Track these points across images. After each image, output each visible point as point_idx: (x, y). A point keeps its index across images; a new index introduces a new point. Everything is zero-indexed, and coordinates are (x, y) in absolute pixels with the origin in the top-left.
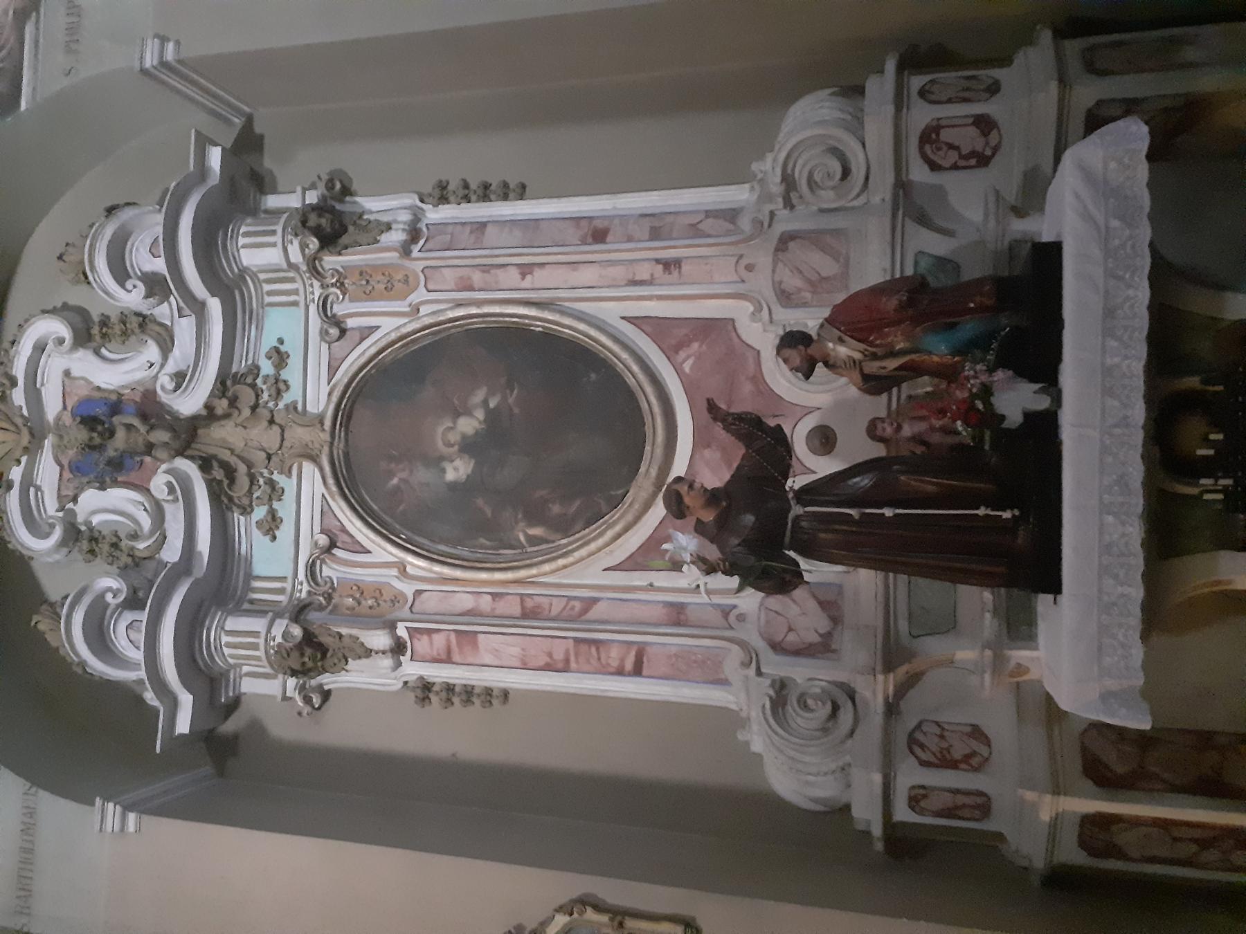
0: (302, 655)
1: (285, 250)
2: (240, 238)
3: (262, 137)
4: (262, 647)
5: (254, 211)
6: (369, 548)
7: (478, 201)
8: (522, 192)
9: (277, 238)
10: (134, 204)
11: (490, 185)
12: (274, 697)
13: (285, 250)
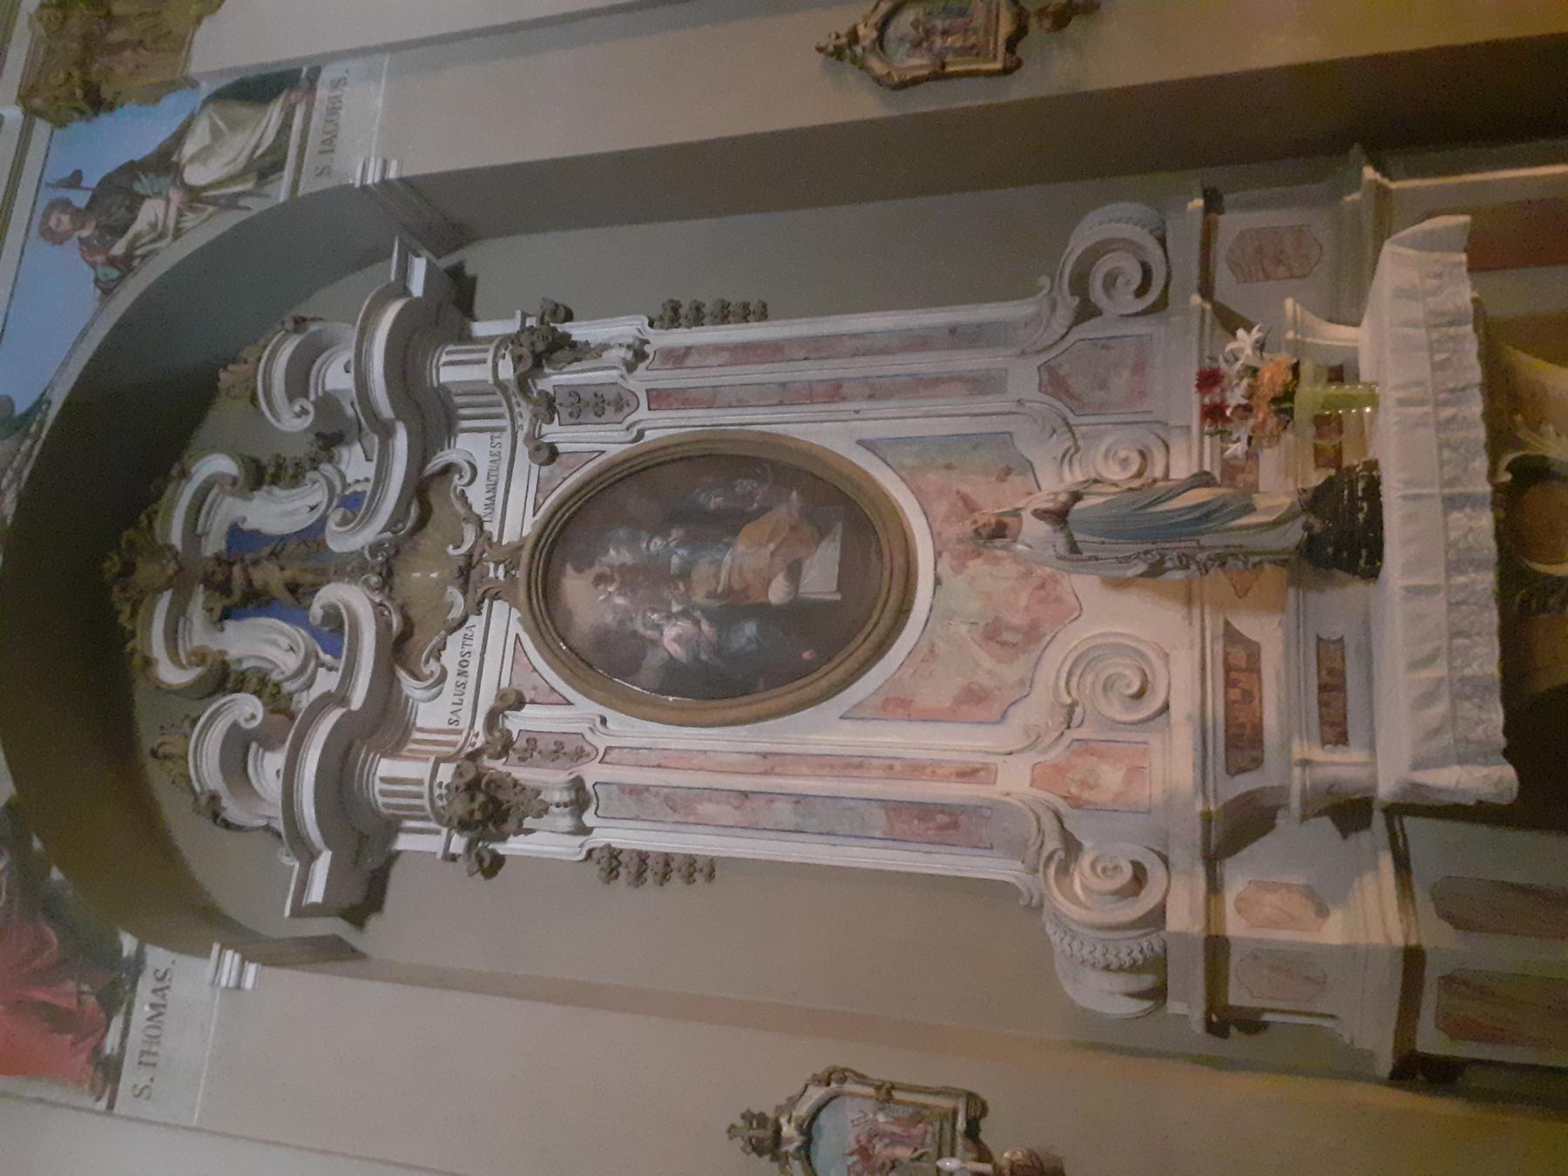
0: (472, 799)
1: (495, 366)
2: (444, 354)
3: (474, 280)
4: (426, 795)
5: (465, 337)
6: (571, 699)
7: (713, 324)
8: (763, 315)
9: (490, 356)
10: (321, 319)
11: (729, 304)
13: (495, 366)
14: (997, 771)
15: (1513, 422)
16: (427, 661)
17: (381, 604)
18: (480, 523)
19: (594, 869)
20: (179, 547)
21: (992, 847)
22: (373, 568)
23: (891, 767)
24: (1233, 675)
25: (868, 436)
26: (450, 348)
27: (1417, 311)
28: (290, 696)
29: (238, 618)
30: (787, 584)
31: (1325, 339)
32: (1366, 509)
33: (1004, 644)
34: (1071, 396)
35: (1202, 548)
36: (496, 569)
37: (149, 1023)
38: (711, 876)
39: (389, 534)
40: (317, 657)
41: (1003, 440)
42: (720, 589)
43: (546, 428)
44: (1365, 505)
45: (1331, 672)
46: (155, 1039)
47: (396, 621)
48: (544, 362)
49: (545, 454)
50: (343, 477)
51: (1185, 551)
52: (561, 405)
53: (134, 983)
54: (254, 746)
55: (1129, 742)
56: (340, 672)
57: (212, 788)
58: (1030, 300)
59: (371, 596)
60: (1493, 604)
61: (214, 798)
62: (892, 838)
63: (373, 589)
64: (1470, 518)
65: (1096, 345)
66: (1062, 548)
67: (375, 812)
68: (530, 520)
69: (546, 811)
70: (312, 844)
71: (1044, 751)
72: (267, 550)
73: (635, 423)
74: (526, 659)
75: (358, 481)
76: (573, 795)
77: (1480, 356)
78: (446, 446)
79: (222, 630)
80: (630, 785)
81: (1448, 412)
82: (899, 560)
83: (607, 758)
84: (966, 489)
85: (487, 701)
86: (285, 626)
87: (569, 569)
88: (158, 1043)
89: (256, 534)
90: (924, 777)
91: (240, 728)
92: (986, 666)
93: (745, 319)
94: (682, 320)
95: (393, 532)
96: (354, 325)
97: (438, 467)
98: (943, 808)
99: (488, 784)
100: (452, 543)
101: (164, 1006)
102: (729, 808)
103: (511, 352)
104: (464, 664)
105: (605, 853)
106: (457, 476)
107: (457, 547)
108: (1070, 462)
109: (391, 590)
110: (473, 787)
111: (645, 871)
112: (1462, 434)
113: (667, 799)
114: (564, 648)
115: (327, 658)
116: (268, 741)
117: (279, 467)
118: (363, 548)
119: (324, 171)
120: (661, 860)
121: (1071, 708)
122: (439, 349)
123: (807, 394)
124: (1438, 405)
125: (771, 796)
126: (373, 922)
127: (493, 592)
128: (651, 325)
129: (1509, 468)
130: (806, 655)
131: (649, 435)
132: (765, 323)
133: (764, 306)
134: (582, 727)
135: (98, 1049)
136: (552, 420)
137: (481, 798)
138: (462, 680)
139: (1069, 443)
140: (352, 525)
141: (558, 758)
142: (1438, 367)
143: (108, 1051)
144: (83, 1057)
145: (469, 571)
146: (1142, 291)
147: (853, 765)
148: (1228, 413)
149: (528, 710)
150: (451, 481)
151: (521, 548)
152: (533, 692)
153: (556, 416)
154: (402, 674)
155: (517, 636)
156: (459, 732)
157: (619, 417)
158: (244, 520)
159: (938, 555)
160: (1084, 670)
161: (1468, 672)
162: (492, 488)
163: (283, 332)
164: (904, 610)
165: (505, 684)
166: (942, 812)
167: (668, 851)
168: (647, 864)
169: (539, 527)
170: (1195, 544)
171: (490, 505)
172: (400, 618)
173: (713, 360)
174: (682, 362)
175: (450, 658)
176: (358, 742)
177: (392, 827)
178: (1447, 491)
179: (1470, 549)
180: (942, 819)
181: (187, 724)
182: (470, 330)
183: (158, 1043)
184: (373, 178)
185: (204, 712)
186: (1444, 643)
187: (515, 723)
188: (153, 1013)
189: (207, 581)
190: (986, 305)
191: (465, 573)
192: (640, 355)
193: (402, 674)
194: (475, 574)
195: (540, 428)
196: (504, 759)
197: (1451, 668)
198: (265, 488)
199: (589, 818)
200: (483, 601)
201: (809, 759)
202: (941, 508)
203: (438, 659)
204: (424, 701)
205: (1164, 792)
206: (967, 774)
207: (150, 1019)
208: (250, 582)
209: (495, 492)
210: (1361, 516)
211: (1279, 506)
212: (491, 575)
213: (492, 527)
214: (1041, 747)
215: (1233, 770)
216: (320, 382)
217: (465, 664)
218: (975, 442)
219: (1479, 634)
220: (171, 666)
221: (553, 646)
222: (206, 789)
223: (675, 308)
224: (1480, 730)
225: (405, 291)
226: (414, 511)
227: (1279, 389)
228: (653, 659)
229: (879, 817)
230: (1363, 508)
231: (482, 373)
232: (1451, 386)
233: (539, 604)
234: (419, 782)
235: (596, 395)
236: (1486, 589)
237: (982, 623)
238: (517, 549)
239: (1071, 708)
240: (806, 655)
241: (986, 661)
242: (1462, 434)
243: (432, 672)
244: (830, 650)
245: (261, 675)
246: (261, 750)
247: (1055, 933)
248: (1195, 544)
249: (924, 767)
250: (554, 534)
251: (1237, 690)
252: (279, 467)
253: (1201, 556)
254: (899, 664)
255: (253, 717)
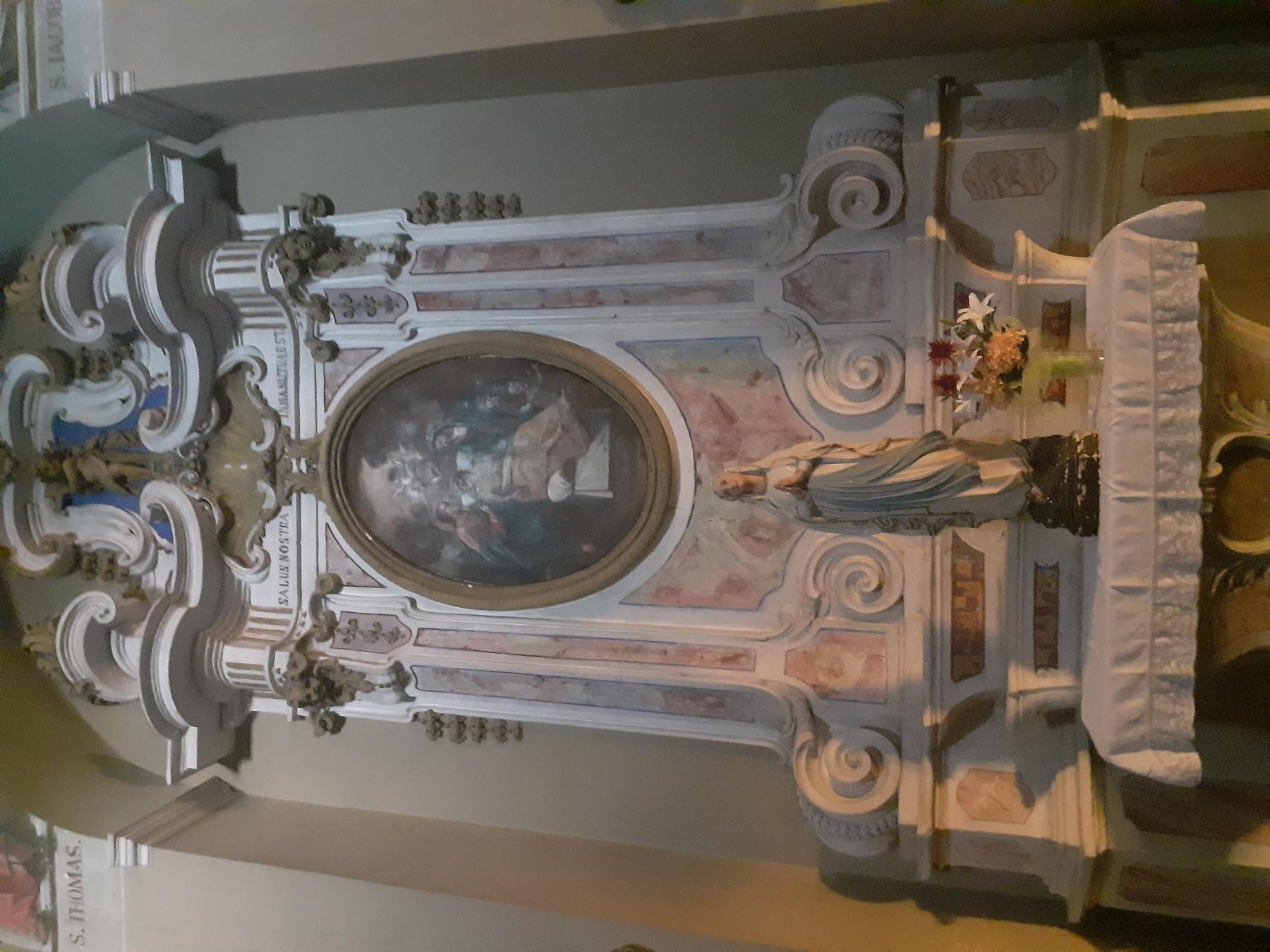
0: (308, 685)
1: (265, 275)
7: (470, 219)
9: (257, 264)
12: (285, 716)
13: (265, 275)
14: (756, 657)
15: (1227, 401)
16: (251, 548)
17: (202, 500)
18: (277, 417)
19: (422, 729)
20: (10, 443)
21: (753, 721)
22: (188, 464)
23: (665, 652)
24: (959, 584)
25: (628, 338)
26: (220, 253)
27: (1143, 305)
28: (139, 578)
29: (79, 504)
30: (564, 481)
31: (1057, 277)
32: (1084, 492)
33: (758, 539)
34: (814, 305)
35: (932, 514)
36: (298, 460)
37: (71, 888)
38: (520, 736)
39: (195, 435)
40: (156, 541)
41: (752, 345)
42: (504, 485)
43: (324, 327)
44: (1084, 488)
45: (1046, 596)
46: (78, 900)
47: (217, 515)
48: (310, 270)
49: (326, 353)
50: (146, 372)
51: (918, 517)
52: (334, 305)
53: (52, 857)
54: (114, 634)
55: (870, 632)
56: (176, 554)
57: (84, 677)
58: (772, 200)
59: (189, 493)
60: (1194, 606)
61: (88, 686)
62: (668, 711)
63: (190, 486)
64: (1180, 522)
65: (836, 259)
66: (803, 509)
67: (225, 686)
68: (322, 416)
69: (373, 689)
70: (179, 724)
71: (797, 638)
72: (90, 443)
73: (406, 323)
74: (337, 546)
75: (160, 376)
76: (394, 677)
77: (1202, 358)
78: (234, 345)
79: (67, 515)
80: (442, 668)
81: (1167, 414)
82: (662, 465)
83: (421, 640)
84: (717, 392)
85: (309, 588)
86: (119, 512)
87: (365, 464)
88: (82, 904)
89: (77, 426)
90: (694, 663)
91: (96, 623)
92: (743, 558)
93: (500, 215)
94: (440, 214)
95: (199, 432)
96: (125, 225)
97: (230, 367)
98: (711, 692)
99: (320, 669)
100: (252, 439)
101: (80, 875)
102: (529, 687)
103: (278, 262)
104: (283, 550)
105: (429, 718)
106: (248, 374)
107: (260, 442)
108: (814, 370)
109: (208, 482)
110: (306, 675)
111: (464, 731)
112: (1180, 438)
113: (475, 679)
114: (370, 538)
115: (163, 542)
116: (124, 626)
117: (85, 360)
118: (175, 449)
119: (59, 83)
120: (477, 724)
121: (818, 602)
122: (210, 256)
123: (567, 299)
124: (1159, 405)
125: (564, 680)
126: (245, 766)
127: (298, 488)
128: (410, 219)
129: (1219, 460)
130: (586, 548)
131: (423, 335)
132: (519, 220)
133: (518, 201)
134: (394, 608)
135: (34, 907)
136: (328, 320)
137: (315, 683)
138: (285, 564)
139: (812, 352)
140: (165, 423)
141: (377, 639)
142: (1160, 366)
143: (43, 908)
144: (26, 910)
145: (274, 466)
146: (880, 210)
147: (631, 649)
148: (959, 387)
149: (346, 591)
150: (245, 378)
151: (317, 444)
152: (349, 576)
153: (332, 315)
154: (231, 562)
155: (327, 524)
156: (290, 611)
157: (391, 317)
158: (65, 411)
159: (697, 456)
160: (830, 564)
161: (1167, 670)
162: (284, 384)
163: (56, 247)
164: (669, 509)
165: (323, 569)
166: (711, 695)
167: (482, 716)
168: (465, 726)
169: (333, 422)
170: (924, 511)
171: (284, 401)
172: (221, 512)
173: (472, 264)
174: (444, 265)
175: (271, 542)
176: (201, 636)
177: (246, 695)
178: (1161, 495)
179: (1177, 554)
180: (711, 700)
181: (50, 625)
182: (237, 225)
183: (82, 904)
184: (107, 96)
185: (63, 611)
186: (1147, 641)
187: (339, 604)
188: (72, 880)
189: (46, 479)
190: (730, 205)
191: (271, 467)
192: (403, 256)
193: (231, 562)
194: (280, 467)
195: (318, 328)
196: (331, 641)
197: (1152, 664)
198: (77, 381)
199: (410, 690)
200: (291, 494)
201: (595, 642)
202: (697, 412)
203: (261, 543)
204: (255, 583)
205: (898, 681)
206: (731, 659)
207: (71, 885)
208: (79, 475)
209: (286, 388)
210: (1079, 499)
211: (1005, 478)
212: (295, 469)
213: (287, 421)
214: (793, 634)
215: (959, 675)
216: (104, 288)
217: (285, 549)
218: (727, 346)
219: (1178, 634)
220: (29, 555)
221: (362, 539)
222: (79, 679)
223: (431, 201)
224: (1172, 723)
225: (168, 199)
226: (214, 410)
227: (1008, 368)
228: (450, 553)
229: (658, 696)
230: (1081, 491)
231: (251, 281)
232: (1172, 387)
233: (342, 499)
234: (259, 668)
235: (365, 297)
236: (1189, 593)
237: (739, 522)
238: (314, 445)
239: (818, 602)
240: (586, 548)
241: (744, 554)
242: (1180, 438)
243: (257, 559)
244: (606, 546)
245: (110, 556)
246: (121, 636)
247: (807, 810)
248: (924, 511)
249: (695, 652)
250: (347, 428)
251: (963, 598)
252: (85, 360)
253: (932, 520)
254: (668, 556)
255: (107, 612)
